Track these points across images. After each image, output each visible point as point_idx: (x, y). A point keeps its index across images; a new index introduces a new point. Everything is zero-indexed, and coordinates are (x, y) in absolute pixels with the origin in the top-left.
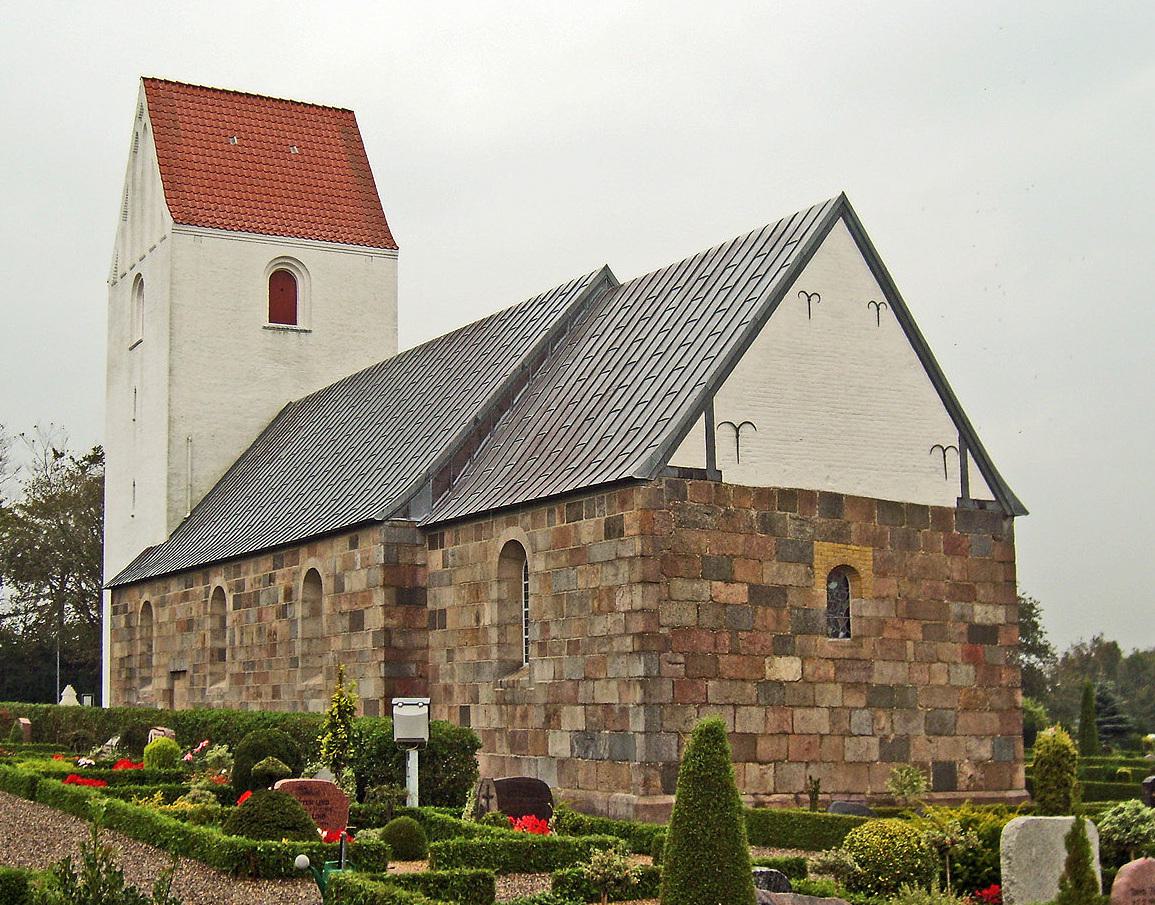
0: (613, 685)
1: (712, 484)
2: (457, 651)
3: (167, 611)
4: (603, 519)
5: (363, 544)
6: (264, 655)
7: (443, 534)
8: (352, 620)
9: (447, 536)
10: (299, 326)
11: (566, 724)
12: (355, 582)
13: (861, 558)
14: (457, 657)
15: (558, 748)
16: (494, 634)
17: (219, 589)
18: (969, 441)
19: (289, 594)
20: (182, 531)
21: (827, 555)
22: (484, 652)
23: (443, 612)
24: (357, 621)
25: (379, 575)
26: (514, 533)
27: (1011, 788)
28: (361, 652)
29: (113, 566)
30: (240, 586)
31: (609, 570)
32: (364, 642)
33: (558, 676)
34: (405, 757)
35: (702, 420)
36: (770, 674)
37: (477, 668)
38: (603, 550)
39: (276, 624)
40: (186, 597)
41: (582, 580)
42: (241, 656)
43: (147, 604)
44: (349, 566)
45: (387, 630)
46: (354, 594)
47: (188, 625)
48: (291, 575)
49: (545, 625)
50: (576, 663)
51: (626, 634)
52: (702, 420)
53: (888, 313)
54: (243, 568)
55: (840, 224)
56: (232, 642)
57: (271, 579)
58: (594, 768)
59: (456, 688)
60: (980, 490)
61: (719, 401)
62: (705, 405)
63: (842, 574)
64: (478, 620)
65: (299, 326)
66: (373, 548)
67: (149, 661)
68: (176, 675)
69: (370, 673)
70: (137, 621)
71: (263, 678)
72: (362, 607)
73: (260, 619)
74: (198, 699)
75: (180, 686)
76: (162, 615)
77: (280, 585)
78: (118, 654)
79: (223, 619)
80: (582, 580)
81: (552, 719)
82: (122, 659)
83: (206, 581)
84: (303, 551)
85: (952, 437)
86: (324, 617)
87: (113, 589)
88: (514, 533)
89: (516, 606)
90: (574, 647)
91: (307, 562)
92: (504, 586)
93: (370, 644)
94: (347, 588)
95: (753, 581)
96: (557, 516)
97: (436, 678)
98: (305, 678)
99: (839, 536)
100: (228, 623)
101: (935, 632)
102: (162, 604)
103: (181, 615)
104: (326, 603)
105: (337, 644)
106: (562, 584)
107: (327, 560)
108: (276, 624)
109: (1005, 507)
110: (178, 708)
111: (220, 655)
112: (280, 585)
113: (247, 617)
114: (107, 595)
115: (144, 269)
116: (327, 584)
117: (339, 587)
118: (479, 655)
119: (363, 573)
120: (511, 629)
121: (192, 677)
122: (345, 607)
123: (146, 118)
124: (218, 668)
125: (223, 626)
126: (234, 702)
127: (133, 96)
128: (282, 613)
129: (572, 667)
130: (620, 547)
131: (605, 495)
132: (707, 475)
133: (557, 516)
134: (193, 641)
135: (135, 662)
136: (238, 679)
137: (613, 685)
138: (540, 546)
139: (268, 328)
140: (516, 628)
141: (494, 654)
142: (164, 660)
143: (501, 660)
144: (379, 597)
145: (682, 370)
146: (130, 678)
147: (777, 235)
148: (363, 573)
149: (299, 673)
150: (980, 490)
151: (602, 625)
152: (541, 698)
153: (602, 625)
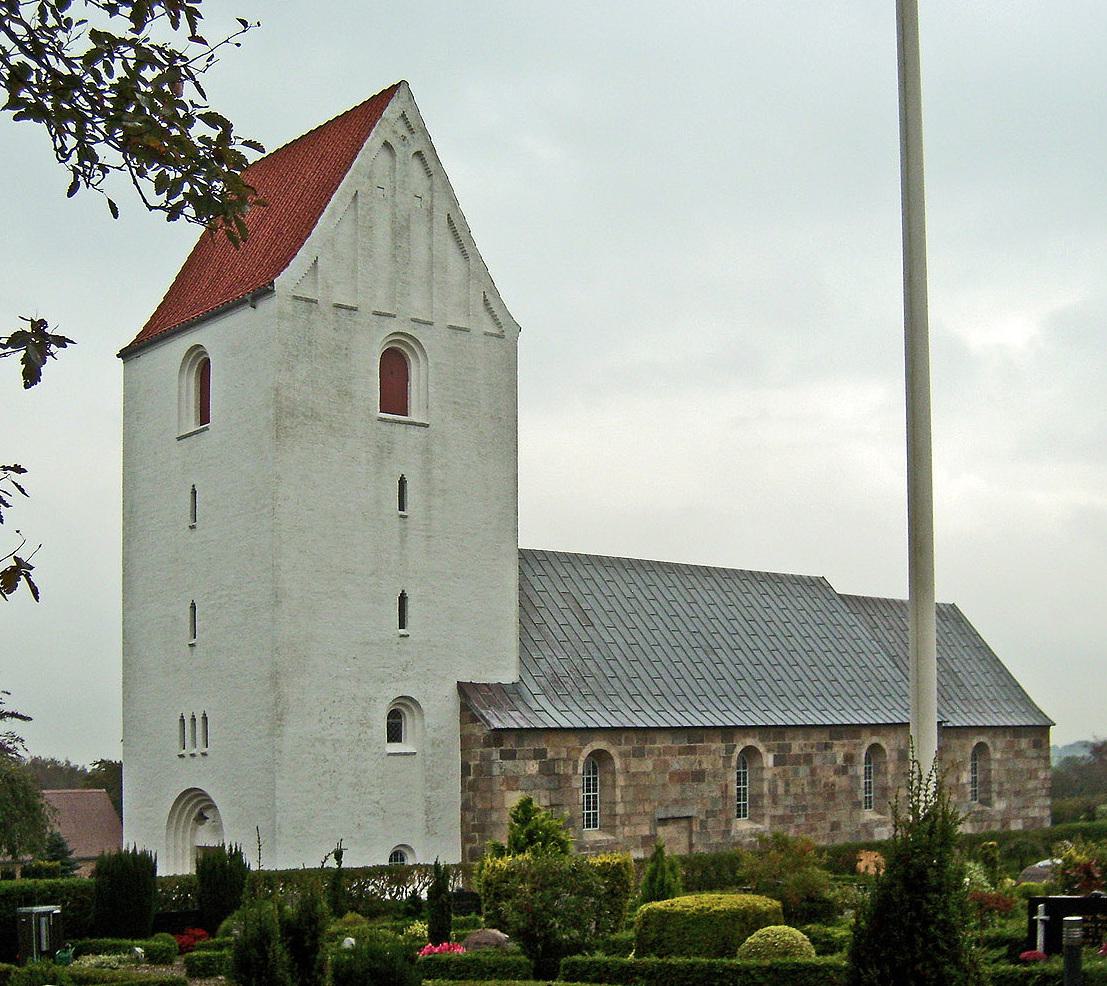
0: (1037, 810)
10: (413, 417)
16: (969, 789)
26: (983, 739)
33: (1009, 807)
41: (1020, 764)
49: (1001, 784)
51: (1044, 788)
64: (958, 779)
65: (413, 417)
80: (1020, 764)
88: (983, 739)
90: (1017, 794)
91: (869, 740)
106: (1010, 765)
129: (1016, 802)
139: (381, 420)
151: (1031, 785)
152: (999, 817)
153: (1031, 785)
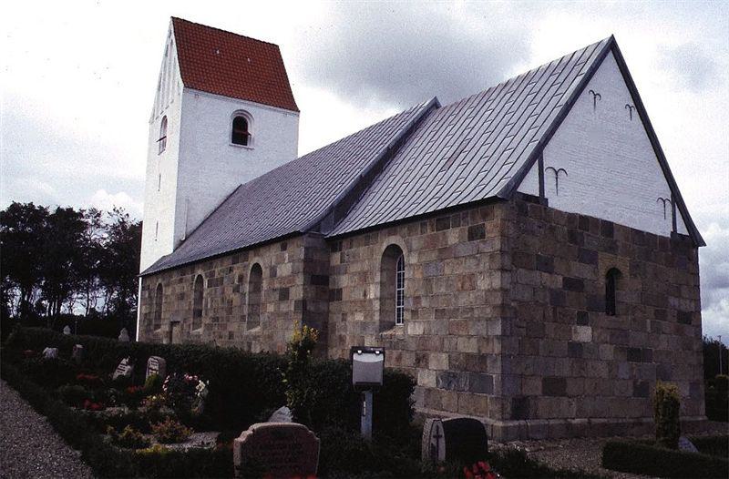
1: (543, 207)
2: (349, 315)
3: (170, 290)
4: (467, 228)
5: (291, 248)
6: (225, 314)
7: (341, 243)
8: (281, 294)
9: (344, 243)
11: (433, 365)
12: (285, 270)
13: (623, 264)
14: (349, 318)
15: (426, 381)
16: (377, 305)
17: (200, 276)
18: (677, 199)
19: (241, 279)
20: (179, 244)
21: (605, 262)
22: (369, 314)
23: (340, 291)
24: (284, 295)
25: (301, 266)
27: (698, 415)
28: (287, 313)
29: (145, 264)
30: (212, 274)
31: (472, 262)
32: (288, 307)
34: (361, 399)
35: (535, 167)
36: (576, 338)
37: (364, 326)
38: (467, 248)
39: (232, 296)
40: (181, 281)
42: (211, 314)
43: (160, 285)
44: (281, 261)
45: (304, 302)
46: (282, 278)
47: (182, 297)
48: (243, 269)
50: (442, 323)
52: (535, 167)
53: (635, 113)
54: (215, 264)
55: (610, 55)
56: (206, 305)
57: (231, 270)
58: (456, 397)
59: (348, 338)
60: (682, 229)
61: (546, 152)
62: (537, 155)
63: (613, 274)
64: (365, 295)
66: (297, 251)
67: (160, 316)
68: (173, 324)
69: (292, 326)
70: (154, 294)
71: (224, 326)
72: (288, 285)
73: (223, 293)
74: (185, 337)
75: (176, 329)
76: (168, 291)
77: (236, 273)
78: (144, 312)
79: (202, 293)
81: (421, 360)
82: (146, 314)
83: (193, 272)
84: (251, 253)
85: (668, 194)
86: (263, 293)
87: (144, 277)
88: (393, 240)
89: (391, 287)
92: (385, 274)
93: (292, 309)
94: (278, 274)
95: (566, 275)
96: (429, 227)
97: (333, 332)
98: (249, 328)
99: (612, 248)
100: (204, 295)
101: (661, 314)
102: (167, 285)
103: (178, 291)
104: (265, 285)
105: (271, 308)
107: (265, 259)
108: (232, 296)
109: (693, 240)
110: (174, 342)
111: (198, 314)
112: (236, 273)
113: (216, 292)
114: (141, 279)
115: (167, 113)
116: (266, 272)
117: (273, 274)
118: (365, 317)
119: (291, 264)
120: (388, 301)
121: (183, 325)
122: (277, 286)
123: (173, 36)
124: (197, 320)
125: (201, 297)
126: (205, 339)
127: (166, 26)
128: (236, 290)
130: (482, 245)
131: (469, 211)
132: (541, 200)
133: (429, 227)
134: (185, 305)
135: (153, 316)
136: (209, 327)
137: (474, 341)
138: (414, 247)
140: (391, 301)
141: (377, 317)
142: (168, 316)
143: (381, 321)
144: (300, 280)
145: (534, 126)
146: (149, 325)
147: (563, 65)
148: (291, 264)
149: (245, 325)
150: (682, 229)
151: (464, 300)
